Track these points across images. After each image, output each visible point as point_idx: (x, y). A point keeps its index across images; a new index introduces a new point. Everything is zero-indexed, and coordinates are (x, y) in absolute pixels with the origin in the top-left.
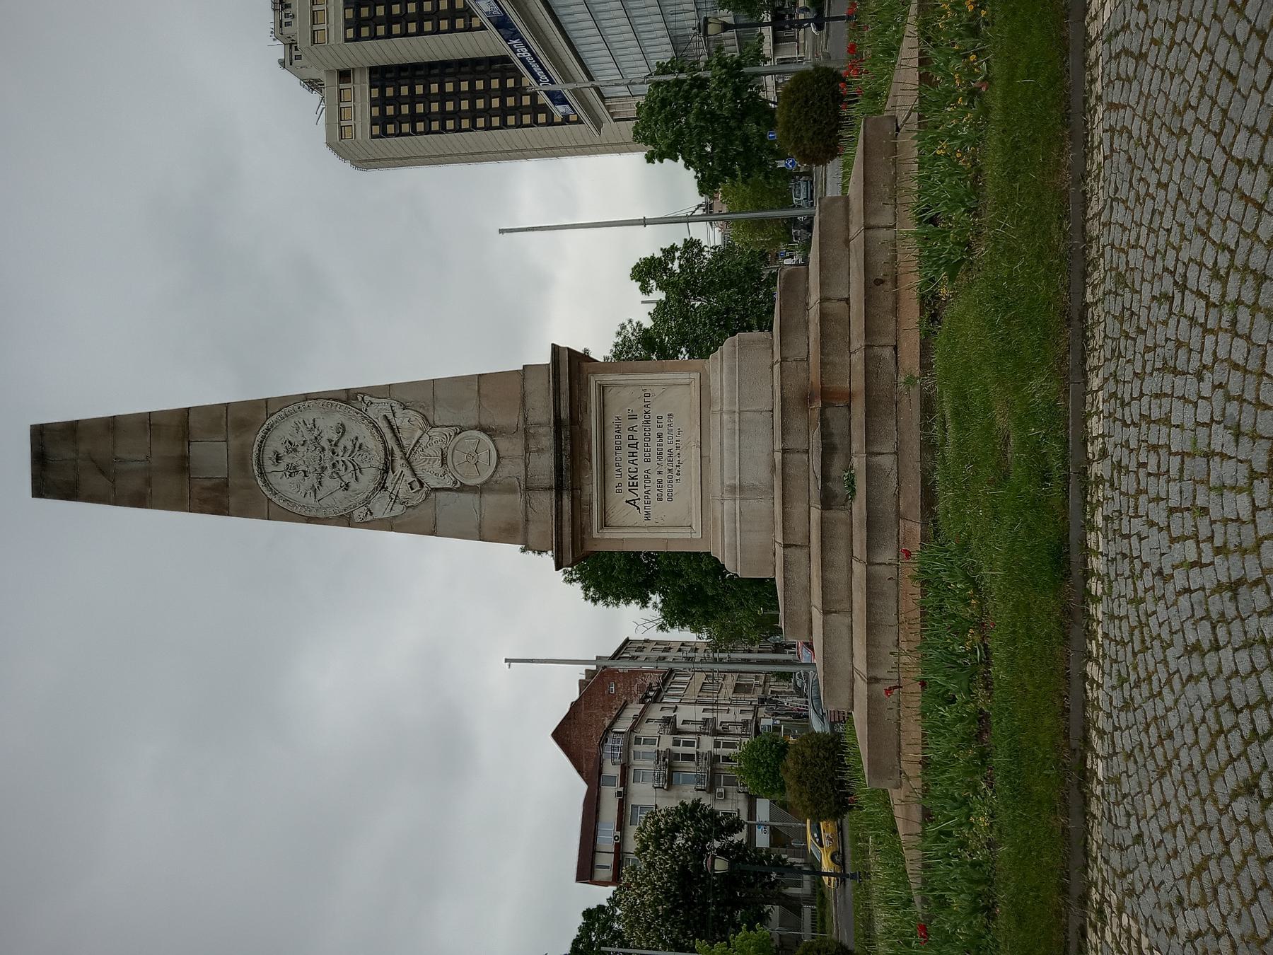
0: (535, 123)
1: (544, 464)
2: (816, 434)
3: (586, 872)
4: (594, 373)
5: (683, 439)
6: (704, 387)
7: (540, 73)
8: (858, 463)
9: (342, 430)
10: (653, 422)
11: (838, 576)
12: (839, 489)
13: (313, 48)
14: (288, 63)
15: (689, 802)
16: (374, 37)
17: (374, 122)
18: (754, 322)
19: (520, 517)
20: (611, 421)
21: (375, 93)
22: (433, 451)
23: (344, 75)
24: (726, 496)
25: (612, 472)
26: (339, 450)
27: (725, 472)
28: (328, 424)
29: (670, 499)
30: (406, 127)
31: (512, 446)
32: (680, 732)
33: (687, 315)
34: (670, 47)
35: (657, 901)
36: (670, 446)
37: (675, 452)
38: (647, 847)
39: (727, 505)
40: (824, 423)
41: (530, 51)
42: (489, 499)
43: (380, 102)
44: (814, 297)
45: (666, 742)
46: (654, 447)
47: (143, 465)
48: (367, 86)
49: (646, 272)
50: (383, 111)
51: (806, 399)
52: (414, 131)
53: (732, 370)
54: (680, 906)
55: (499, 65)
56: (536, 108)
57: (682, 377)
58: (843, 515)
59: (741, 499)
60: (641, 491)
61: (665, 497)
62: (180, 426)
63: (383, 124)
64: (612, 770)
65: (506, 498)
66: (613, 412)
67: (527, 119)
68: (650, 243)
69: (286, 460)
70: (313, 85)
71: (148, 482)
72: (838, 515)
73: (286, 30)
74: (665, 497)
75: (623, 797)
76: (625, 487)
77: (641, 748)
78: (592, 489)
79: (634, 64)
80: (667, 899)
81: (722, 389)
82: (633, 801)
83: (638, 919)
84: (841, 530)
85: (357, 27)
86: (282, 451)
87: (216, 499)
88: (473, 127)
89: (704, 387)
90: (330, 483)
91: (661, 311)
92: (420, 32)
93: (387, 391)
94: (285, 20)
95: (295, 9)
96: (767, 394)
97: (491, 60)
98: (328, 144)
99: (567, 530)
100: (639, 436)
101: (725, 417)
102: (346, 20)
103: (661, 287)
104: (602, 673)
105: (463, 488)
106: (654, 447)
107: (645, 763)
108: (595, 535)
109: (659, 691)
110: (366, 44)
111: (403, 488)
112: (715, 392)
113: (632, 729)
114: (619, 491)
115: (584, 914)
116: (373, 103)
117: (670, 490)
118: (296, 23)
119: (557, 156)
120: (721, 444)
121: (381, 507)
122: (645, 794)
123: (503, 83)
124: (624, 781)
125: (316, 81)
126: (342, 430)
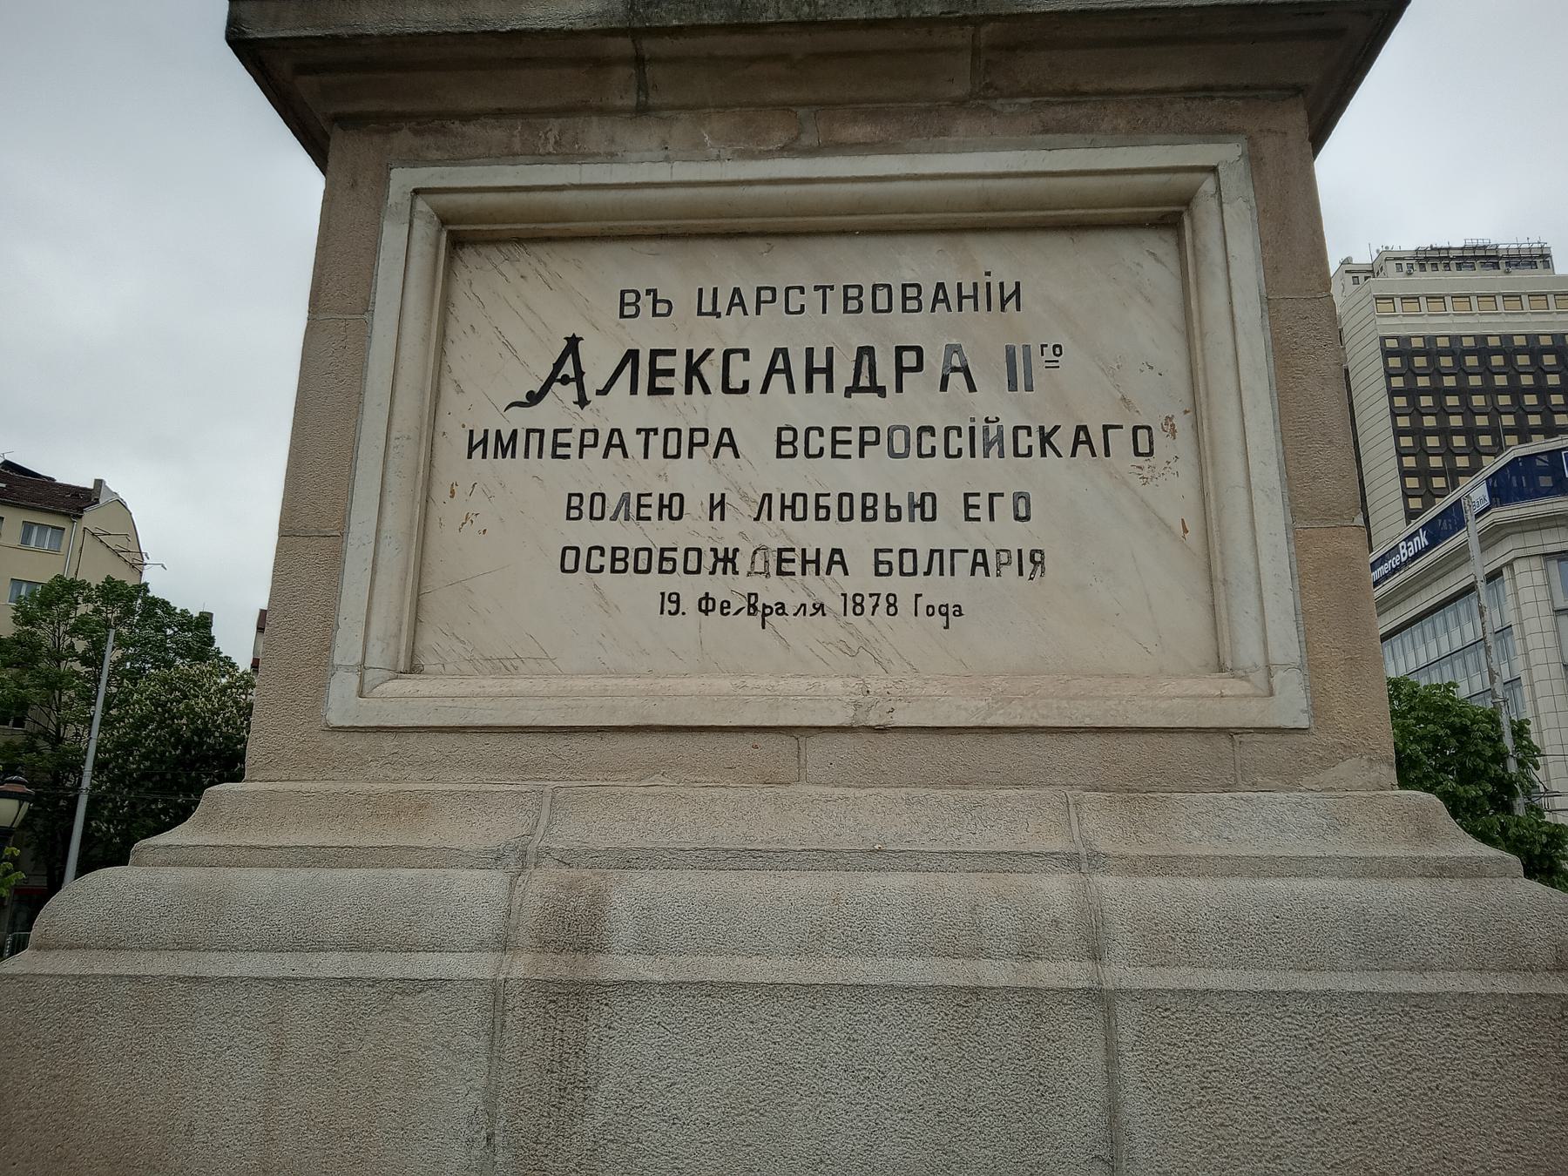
4: (1254, 160)
5: (906, 634)
6: (1225, 752)
10: (993, 473)
14: (1348, 267)
16: (1389, 374)
20: (996, 261)
24: (541, 883)
25: (732, 269)
29: (572, 560)
35: (191, 714)
36: (859, 561)
37: (827, 588)
39: (478, 888)
54: (187, 749)
57: (1270, 620)
59: (497, 992)
60: (626, 410)
61: (585, 533)
66: (1052, 275)
73: (1392, 265)
74: (585, 533)
76: (646, 334)
80: (196, 732)
81: (1235, 867)
94: (1404, 263)
95: (1419, 276)
100: (919, 402)
101: (1056, 887)
102: (1408, 339)
108: (402, 179)
110: (1380, 363)
114: (627, 305)
117: (620, 560)
118: (1400, 277)
120: (878, 858)
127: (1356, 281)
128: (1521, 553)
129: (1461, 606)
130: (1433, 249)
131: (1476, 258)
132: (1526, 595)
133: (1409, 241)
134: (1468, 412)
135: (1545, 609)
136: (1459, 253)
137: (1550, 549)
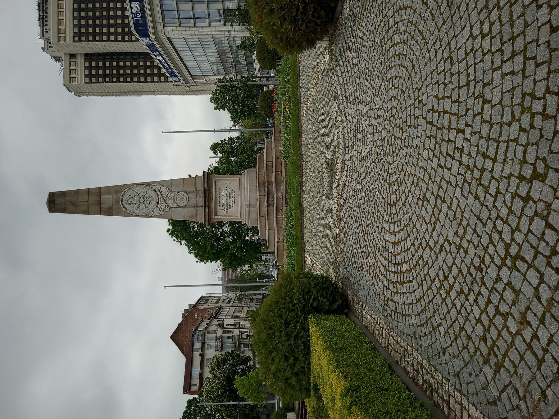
0: (160, 81)
1: (201, 201)
2: (266, 191)
3: (187, 389)
7: (166, 65)
8: (275, 196)
9: (146, 192)
10: (228, 190)
11: (271, 222)
12: (271, 202)
13: (58, 44)
14: (46, 49)
15: (230, 351)
17: (86, 76)
18: (253, 165)
19: (195, 214)
20: (217, 190)
21: (76, 6)
22: (171, 198)
23: (73, 56)
25: (218, 202)
26: (145, 198)
27: (246, 201)
28: (142, 191)
30: (101, 80)
31: (192, 196)
32: (225, 329)
33: (229, 162)
34: (217, 54)
35: (218, 389)
38: (214, 369)
40: (268, 188)
41: (162, 57)
42: (186, 209)
43: (90, 68)
44: (265, 161)
45: (220, 332)
46: (228, 195)
47: (87, 203)
48: (83, 61)
49: (215, 147)
50: (80, 14)
51: (264, 184)
52: (105, 81)
53: (247, 177)
55: (145, 56)
56: (160, 75)
58: (272, 208)
60: (225, 207)
62: (99, 192)
63: (90, 77)
64: (198, 345)
65: (191, 209)
66: (218, 187)
67: (156, 79)
68: (218, 138)
69: (130, 201)
70: (57, 59)
71: (88, 208)
72: (271, 208)
75: (202, 356)
77: (210, 335)
78: (213, 206)
79: (198, 51)
82: (207, 357)
83: (211, 397)
84: (272, 212)
85: (79, 36)
86: (128, 198)
87: (109, 211)
88: (132, 81)
89: (240, 181)
90: (142, 206)
91: (221, 161)
92: (109, 40)
93: (158, 182)
94: (45, 31)
96: (255, 183)
97: (140, 54)
98: (64, 85)
99: (207, 216)
100: (225, 193)
103: (220, 152)
104: (192, 310)
105: (179, 207)
106: (228, 195)
107: (211, 341)
109: (217, 314)
111: (163, 207)
112: (243, 182)
113: (206, 329)
115: (187, 402)
116: (86, 68)
119: (169, 95)
121: (157, 212)
122: (211, 353)
123: (145, 63)
124: (203, 349)
125: (59, 57)
126: (146, 192)
127: (51, 47)
128: (163, 33)
129: (173, 40)
130: (39, 20)
131: (43, 7)
132: (175, 33)
133: (36, 28)
134: (101, 17)
135: (179, 29)
136: (41, 12)
137: (162, 26)
